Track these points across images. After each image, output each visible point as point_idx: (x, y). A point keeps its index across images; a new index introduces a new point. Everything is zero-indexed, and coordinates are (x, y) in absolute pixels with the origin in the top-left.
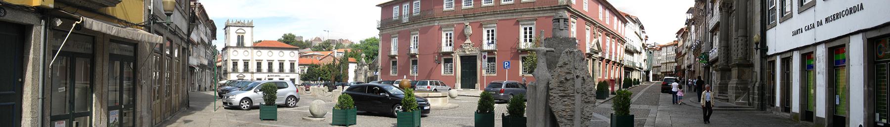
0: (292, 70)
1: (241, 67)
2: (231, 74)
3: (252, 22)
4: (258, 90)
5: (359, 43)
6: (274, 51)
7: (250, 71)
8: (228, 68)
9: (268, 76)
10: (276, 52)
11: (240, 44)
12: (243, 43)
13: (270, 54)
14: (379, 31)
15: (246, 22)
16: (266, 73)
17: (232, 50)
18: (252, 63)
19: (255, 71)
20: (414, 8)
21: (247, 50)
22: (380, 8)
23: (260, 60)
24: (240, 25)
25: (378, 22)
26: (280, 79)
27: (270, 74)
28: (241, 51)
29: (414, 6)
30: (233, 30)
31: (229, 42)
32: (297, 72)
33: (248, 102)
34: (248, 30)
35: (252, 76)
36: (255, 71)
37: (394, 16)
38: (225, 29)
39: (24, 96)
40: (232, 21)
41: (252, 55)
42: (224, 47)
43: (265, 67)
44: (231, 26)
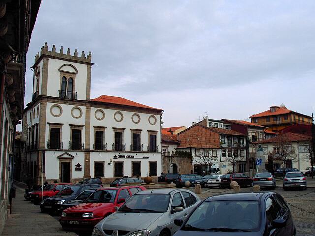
0: (152, 149)
1: (66, 138)
2: (91, 154)
3: (89, 56)
5: (249, 121)
7: (84, 147)
9: (115, 157)
10: (110, 113)
11: (67, 96)
12: (72, 94)
13: (136, 119)
15: (58, 51)
16: (111, 152)
17: (49, 105)
18: (88, 133)
19: (91, 148)
23: (101, 127)
26: (147, 158)
27: (117, 154)
28: (67, 108)
30: (54, 65)
31: (45, 86)
32: (40, 152)
34: (82, 68)
35: (86, 158)
36: (91, 148)
39: (296, 192)
41: (88, 117)
43: (109, 140)
44: (51, 57)
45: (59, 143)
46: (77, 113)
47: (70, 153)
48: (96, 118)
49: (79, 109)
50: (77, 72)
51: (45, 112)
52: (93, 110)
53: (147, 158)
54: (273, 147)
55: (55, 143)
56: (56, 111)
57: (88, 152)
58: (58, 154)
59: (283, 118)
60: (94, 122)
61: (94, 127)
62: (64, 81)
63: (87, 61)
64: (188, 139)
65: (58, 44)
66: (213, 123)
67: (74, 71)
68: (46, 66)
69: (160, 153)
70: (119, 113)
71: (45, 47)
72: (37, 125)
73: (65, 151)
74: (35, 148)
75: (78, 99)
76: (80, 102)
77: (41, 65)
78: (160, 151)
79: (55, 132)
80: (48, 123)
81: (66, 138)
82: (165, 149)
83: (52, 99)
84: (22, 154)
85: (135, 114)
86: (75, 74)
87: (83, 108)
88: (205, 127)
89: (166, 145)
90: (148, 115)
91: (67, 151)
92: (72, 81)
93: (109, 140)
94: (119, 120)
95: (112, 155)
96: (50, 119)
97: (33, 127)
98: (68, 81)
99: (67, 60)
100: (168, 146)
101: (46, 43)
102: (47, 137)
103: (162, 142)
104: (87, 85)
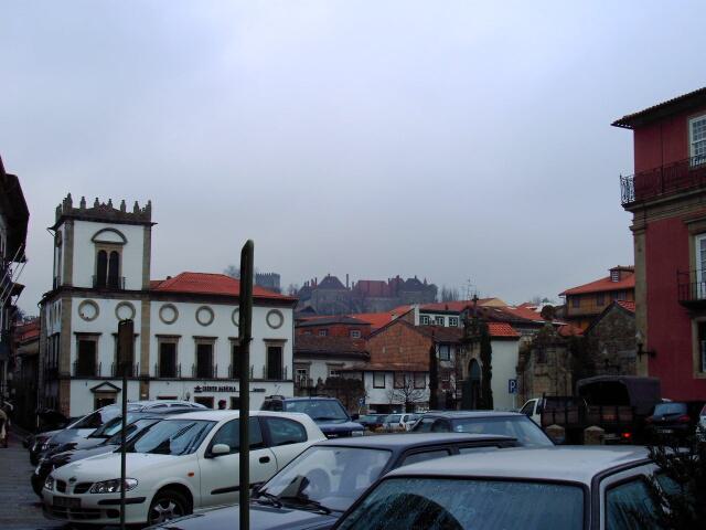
4: (226, 447)
6: (182, 307)
7: (139, 372)
8: (63, 362)
9: (198, 390)
10: (187, 310)
13: (205, 316)
14: (631, 215)
15: (130, 209)
17: (77, 301)
18: (145, 347)
19: (152, 373)
20: (692, 141)
21: (94, 300)
22: (630, 133)
24: (103, 214)
25: (624, 183)
26: (263, 391)
27: (201, 385)
29: (691, 136)
33: (172, 506)
34: (134, 234)
36: (152, 373)
37: (692, 154)
38: (55, 228)
40: (83, 202)
42: (50, 288)
43: (186, 358)
45: (211, 367)
46: (275, 320)
47: (112, 382)
48: (158, 321)
49: (130, 306)
50: (125, 242)
51: (70, 315)
52: (156, 306)
53: (263, 391)
54: (93, 390)
55: (87, 367)
56: (89, 311)
57: (145, 380)
58: (93, 384)
59: (594, 302)
60: (158, 327)
61: (157, 336)
62: (101, 257)
63: (142, 218)
64: (384, 351)
65: (89, 193)
66: (432, 317)
67: (120, 240)
68: (70, 233)
69: (290, 381)
70: (206, 308)
71: (68, 200)
72: (58, 334)
73: (104, 379)
74: (56, 376)
75: (128, 287)
76: (133, 294)
77: (62, 228)
78: (290, 376)
79: (88, 344)
80: (75, 333)
81: (106, 356)
82: (301, 370)
83: (81, 291)
84: (40, 383)
85: (86, 303)
86: (120, 245)
87: (138, 304)
88: (411, 325)
89: (337, 362)
90: (194, 307)
91: (109, 379)
92: (116, 257)
93: (186, 358)
94: (169, 319)
95: (191, 386)
96: (78, 325)
97: (54, 336)
98: (108, 262)
99: (107, 221)
100: (309, 364)
101: (150, 202)
102: (73, 356)
103: (296, 355)
104: (144, 263)
